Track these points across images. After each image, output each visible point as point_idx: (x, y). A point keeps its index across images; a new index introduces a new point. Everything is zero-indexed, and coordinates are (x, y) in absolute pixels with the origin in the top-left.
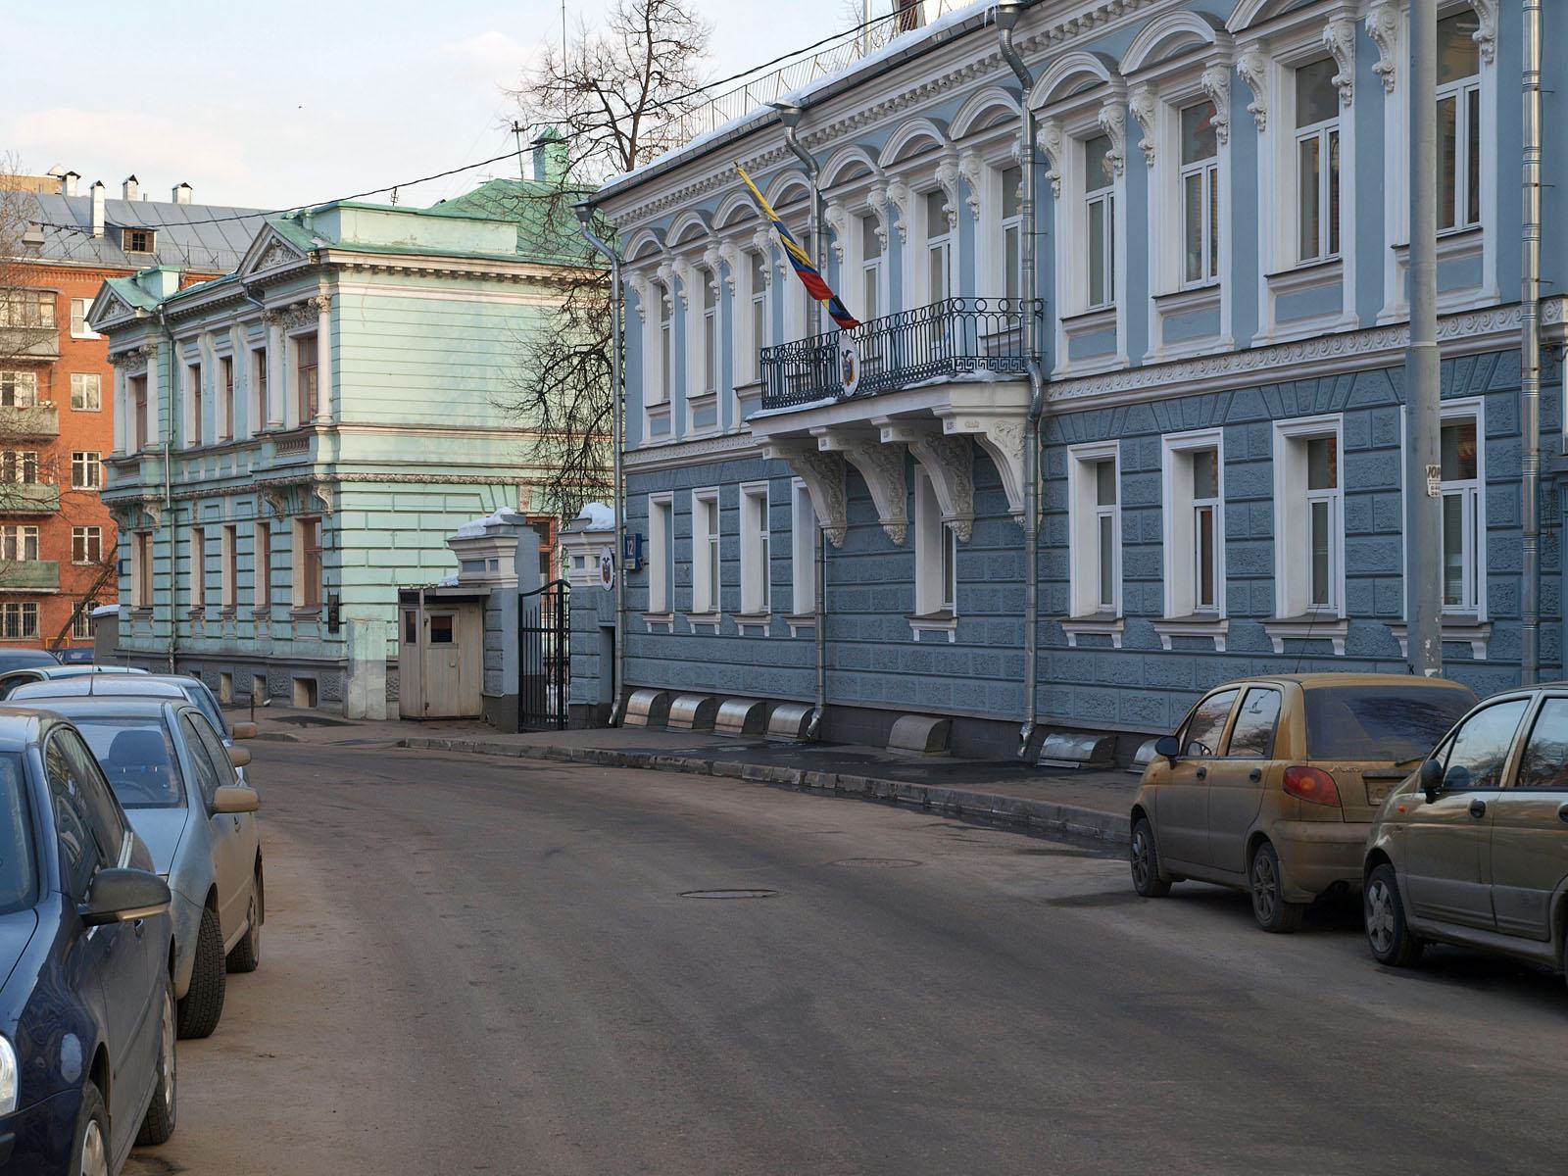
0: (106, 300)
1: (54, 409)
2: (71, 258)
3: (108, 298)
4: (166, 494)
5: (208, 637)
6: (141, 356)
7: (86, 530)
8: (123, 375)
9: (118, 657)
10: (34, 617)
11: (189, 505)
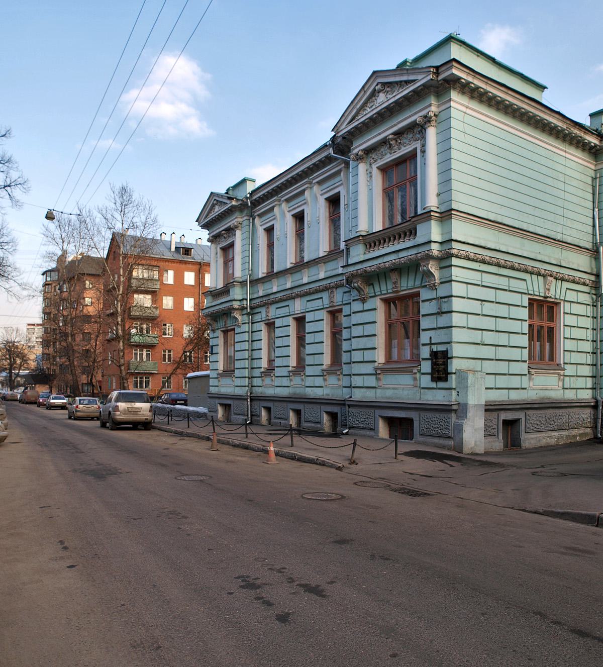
0: (211, 203)
1: (157, 308)
2: (164, 256)
3: (212, 202)
4: (247, 304)
5: (277, 386)
6: (230, 231)
7: (167, 351)
8: (216, 248)
9: (210, 397)
10: (148, 381)
11: (263, 310)
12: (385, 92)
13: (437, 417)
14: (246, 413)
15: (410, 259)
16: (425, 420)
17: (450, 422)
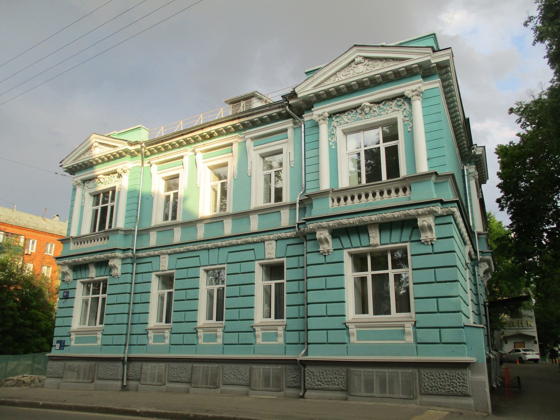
12: (365, 65)
13: (447, 374)
14: (120, 377)
15: (188, 249)
16: (428, 378)
17: (467, 379)
